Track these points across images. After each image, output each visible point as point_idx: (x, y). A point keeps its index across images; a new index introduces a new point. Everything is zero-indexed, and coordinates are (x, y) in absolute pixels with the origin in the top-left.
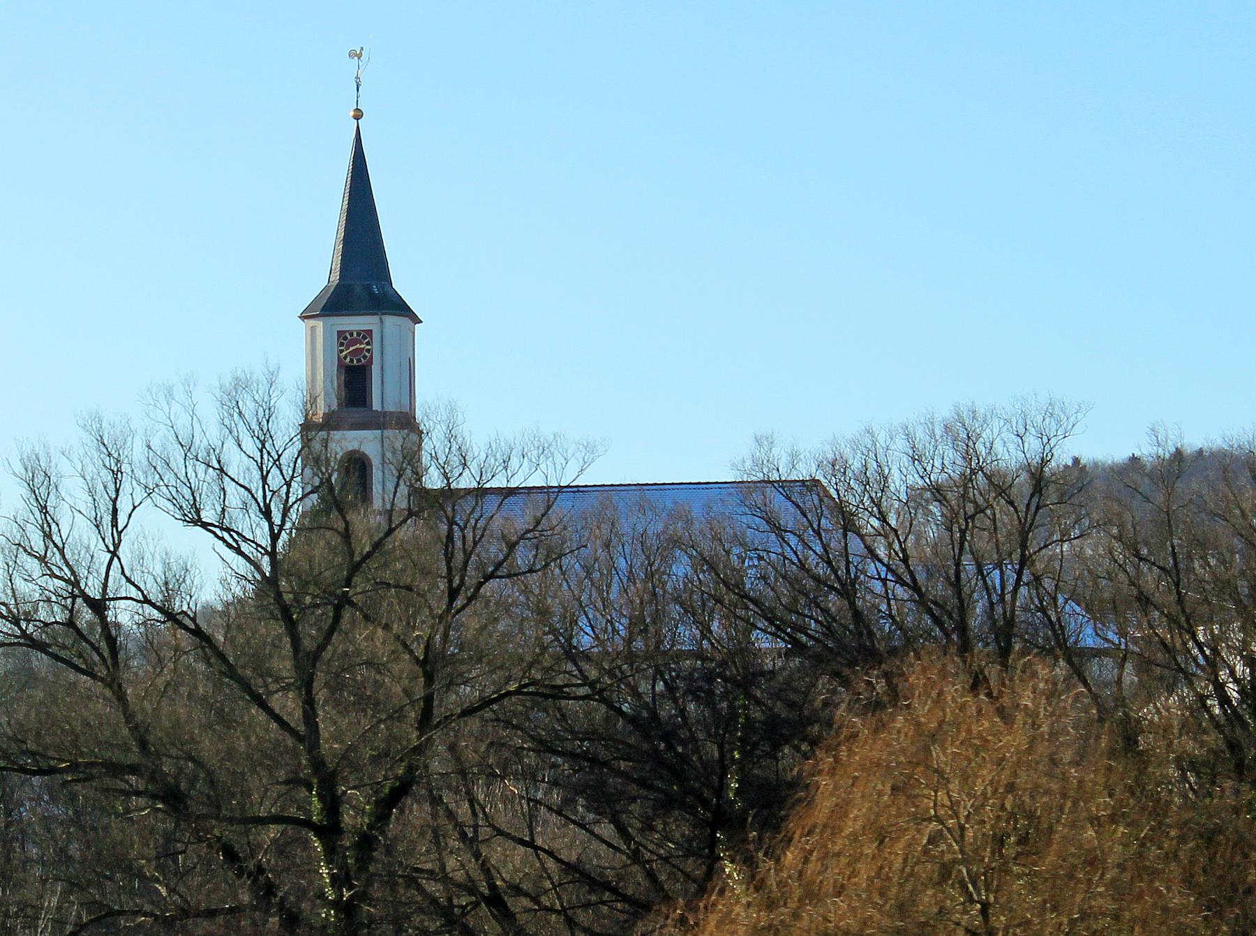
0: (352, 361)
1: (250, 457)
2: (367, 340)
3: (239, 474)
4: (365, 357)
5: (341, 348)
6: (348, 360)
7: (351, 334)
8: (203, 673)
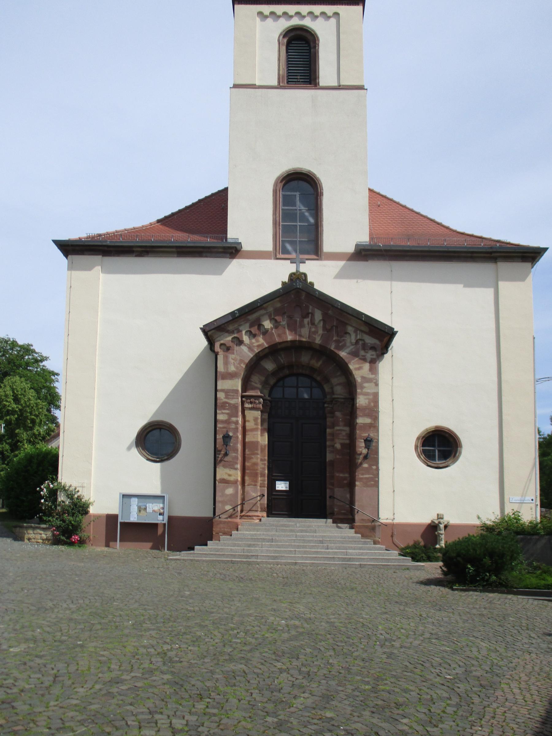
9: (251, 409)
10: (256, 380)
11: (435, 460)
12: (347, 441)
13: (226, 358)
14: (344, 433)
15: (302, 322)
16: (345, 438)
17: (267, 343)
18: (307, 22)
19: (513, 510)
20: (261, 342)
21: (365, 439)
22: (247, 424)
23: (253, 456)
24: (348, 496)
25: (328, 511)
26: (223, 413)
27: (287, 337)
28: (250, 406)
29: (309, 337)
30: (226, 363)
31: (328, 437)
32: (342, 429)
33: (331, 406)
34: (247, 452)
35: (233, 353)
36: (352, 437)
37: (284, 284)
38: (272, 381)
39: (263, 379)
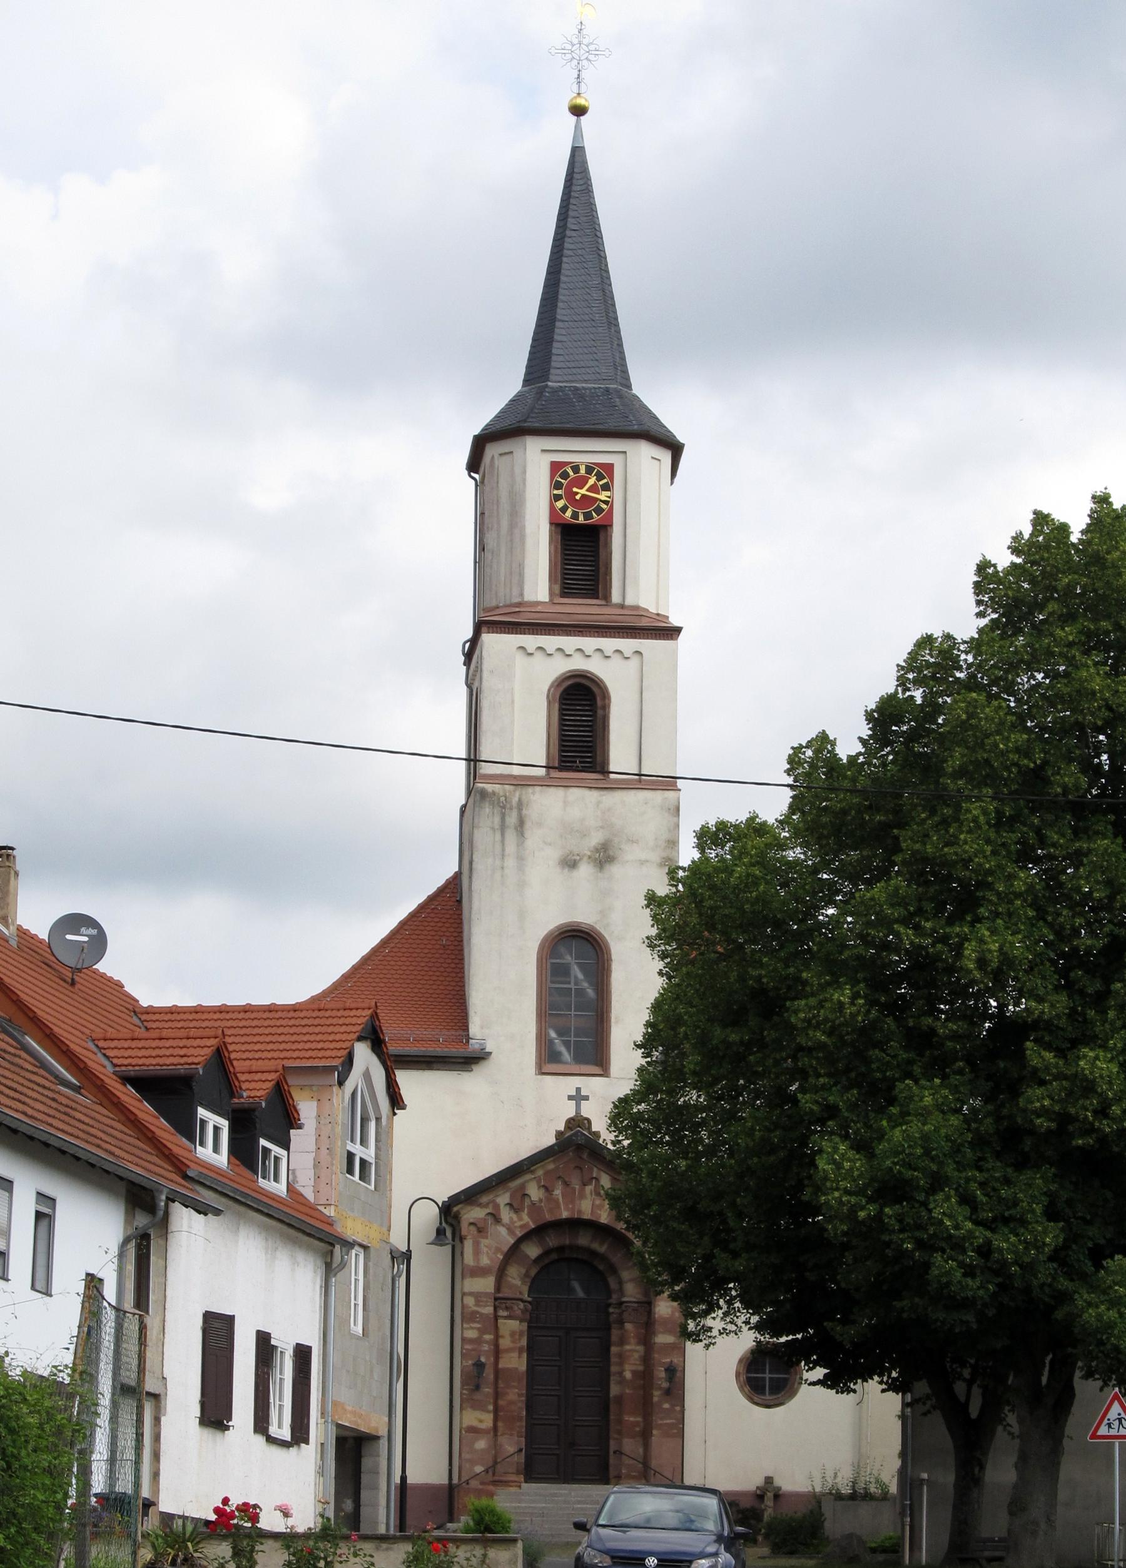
0: (575, 515)
1: (126, 1049)
2: (605, 481)
3: (44, 1219)
4: (599, 510)
5: (556, 492)
6: (569, 514)
7: (576, 469)
8: (1122, 988)
9: (506, 1318)
10: (516, 1277)
11: (764, 1394)
12: (641, 1368)
13: (476, 1244)
14: (636, 1355)
15: (582, 1191)
16: (638, 1363)
17: (534, 1222)
18: (595, 667)
19: (286, 1514)
20: (526, 1221)
21: (666, 1366)
22: (501, 1341)
23: (508, 1391)
24: (641, 1450)
25: (612, 1472)
26: (472, 1328)
27: (561, 1214)
28: (505, 1314)
29: (591, 1214)
30: (477, 1252)
31: (613, 1359)
32: (633, 1349)
33: (617, 1311)
34: (501, 1385)
35: (487, 1238)
36: (647, 1359)
37: (559, 1134)
38: (533, 1272)
39: (523, 1271)
